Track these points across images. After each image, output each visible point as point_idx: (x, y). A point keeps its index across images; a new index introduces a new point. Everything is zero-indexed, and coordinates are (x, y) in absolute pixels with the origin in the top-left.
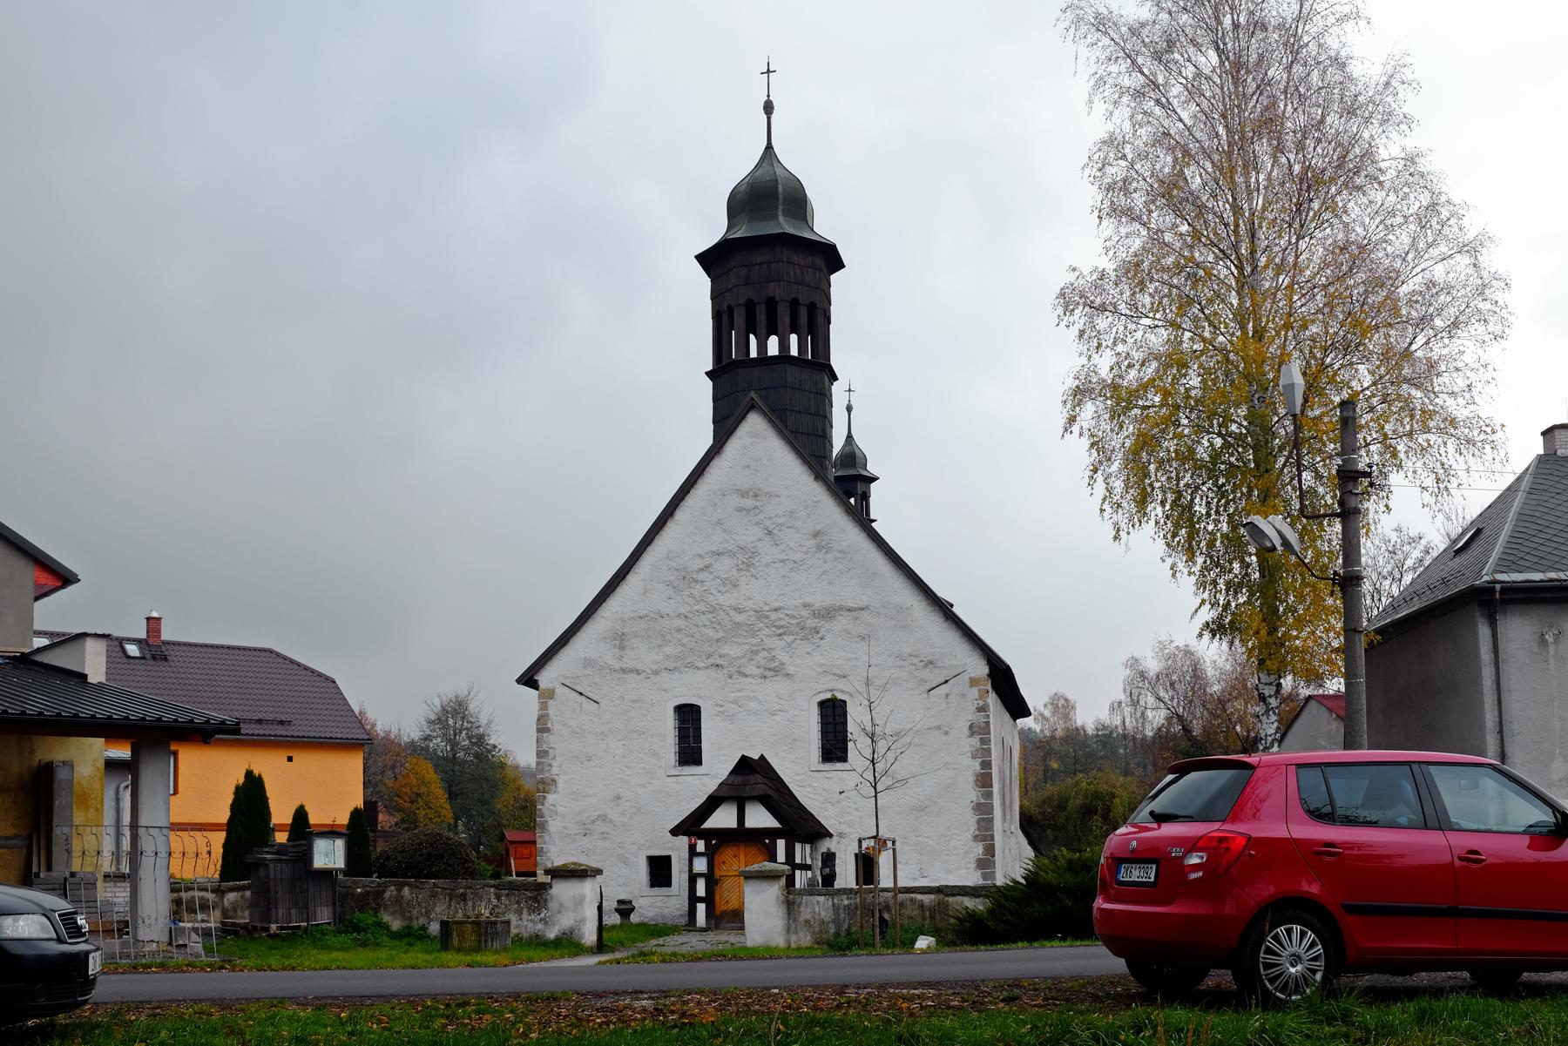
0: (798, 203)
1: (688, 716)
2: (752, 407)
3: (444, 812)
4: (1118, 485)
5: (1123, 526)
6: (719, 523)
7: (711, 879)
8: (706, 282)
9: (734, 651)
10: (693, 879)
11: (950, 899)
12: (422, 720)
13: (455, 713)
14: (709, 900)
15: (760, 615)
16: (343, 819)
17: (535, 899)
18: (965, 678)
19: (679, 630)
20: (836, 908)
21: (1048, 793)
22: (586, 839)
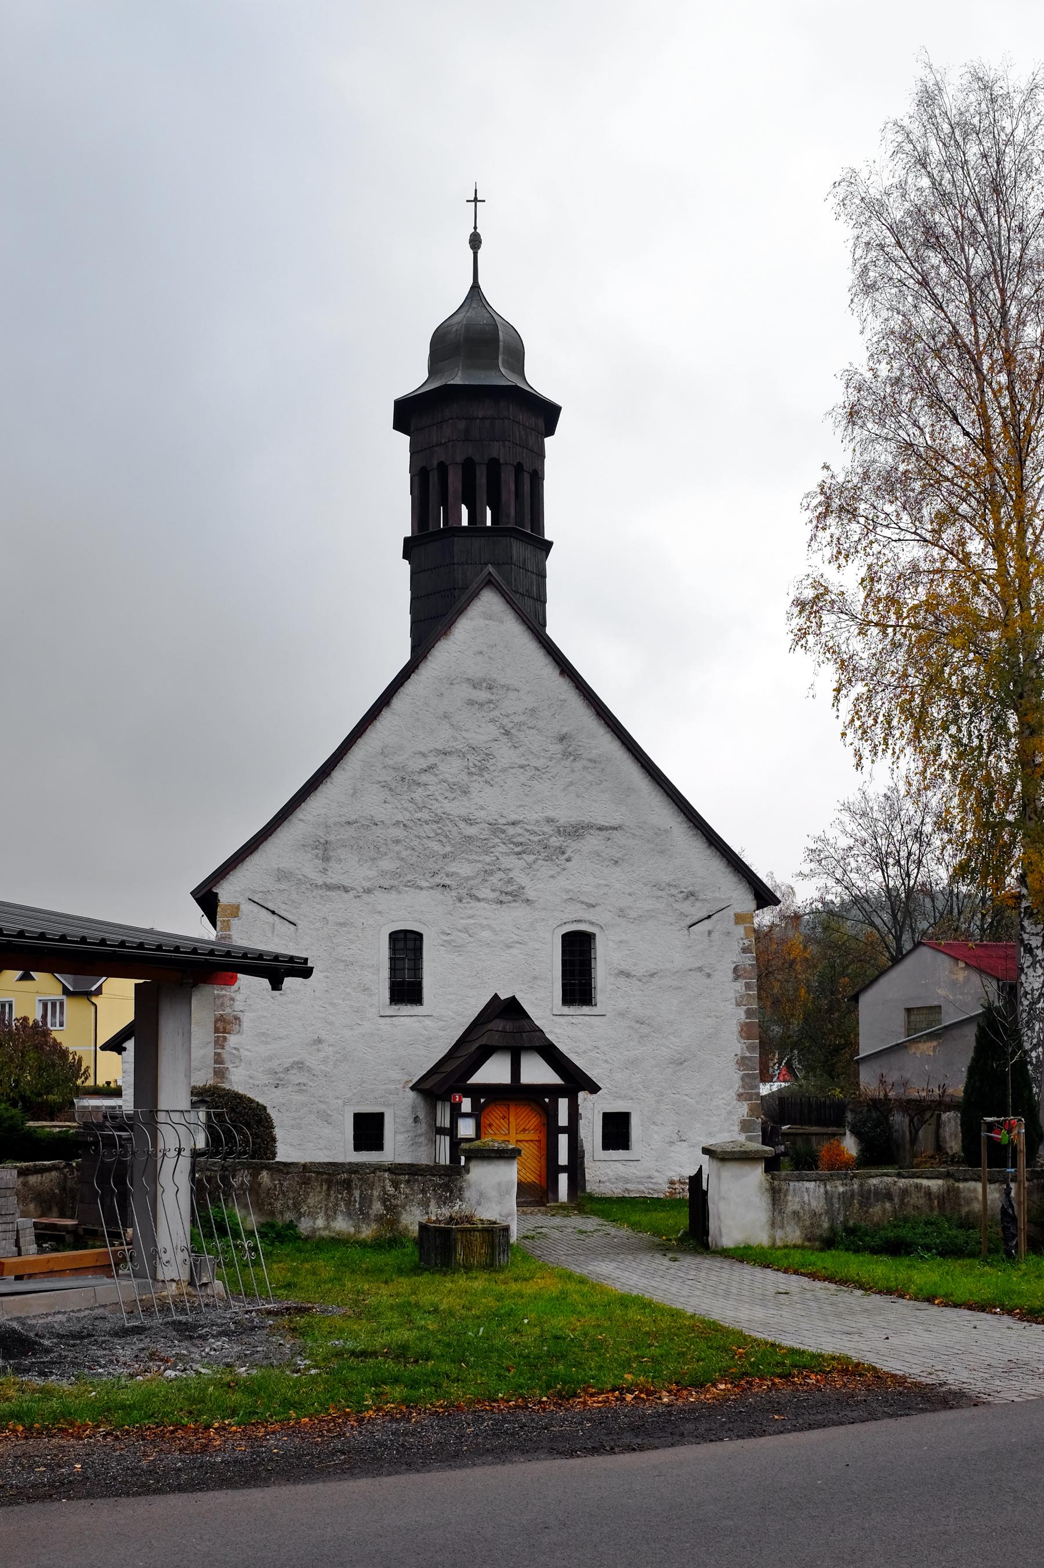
1: (406, 947)
5: (866, 753)
6: (446, 716)
9: (464, 869)
11: (961, 1185)
15: (495, 828)
17: (447, 1187)
18: (730, 913)
19: (398, 842)
20: (828, 1197)
22: (278, 1092)
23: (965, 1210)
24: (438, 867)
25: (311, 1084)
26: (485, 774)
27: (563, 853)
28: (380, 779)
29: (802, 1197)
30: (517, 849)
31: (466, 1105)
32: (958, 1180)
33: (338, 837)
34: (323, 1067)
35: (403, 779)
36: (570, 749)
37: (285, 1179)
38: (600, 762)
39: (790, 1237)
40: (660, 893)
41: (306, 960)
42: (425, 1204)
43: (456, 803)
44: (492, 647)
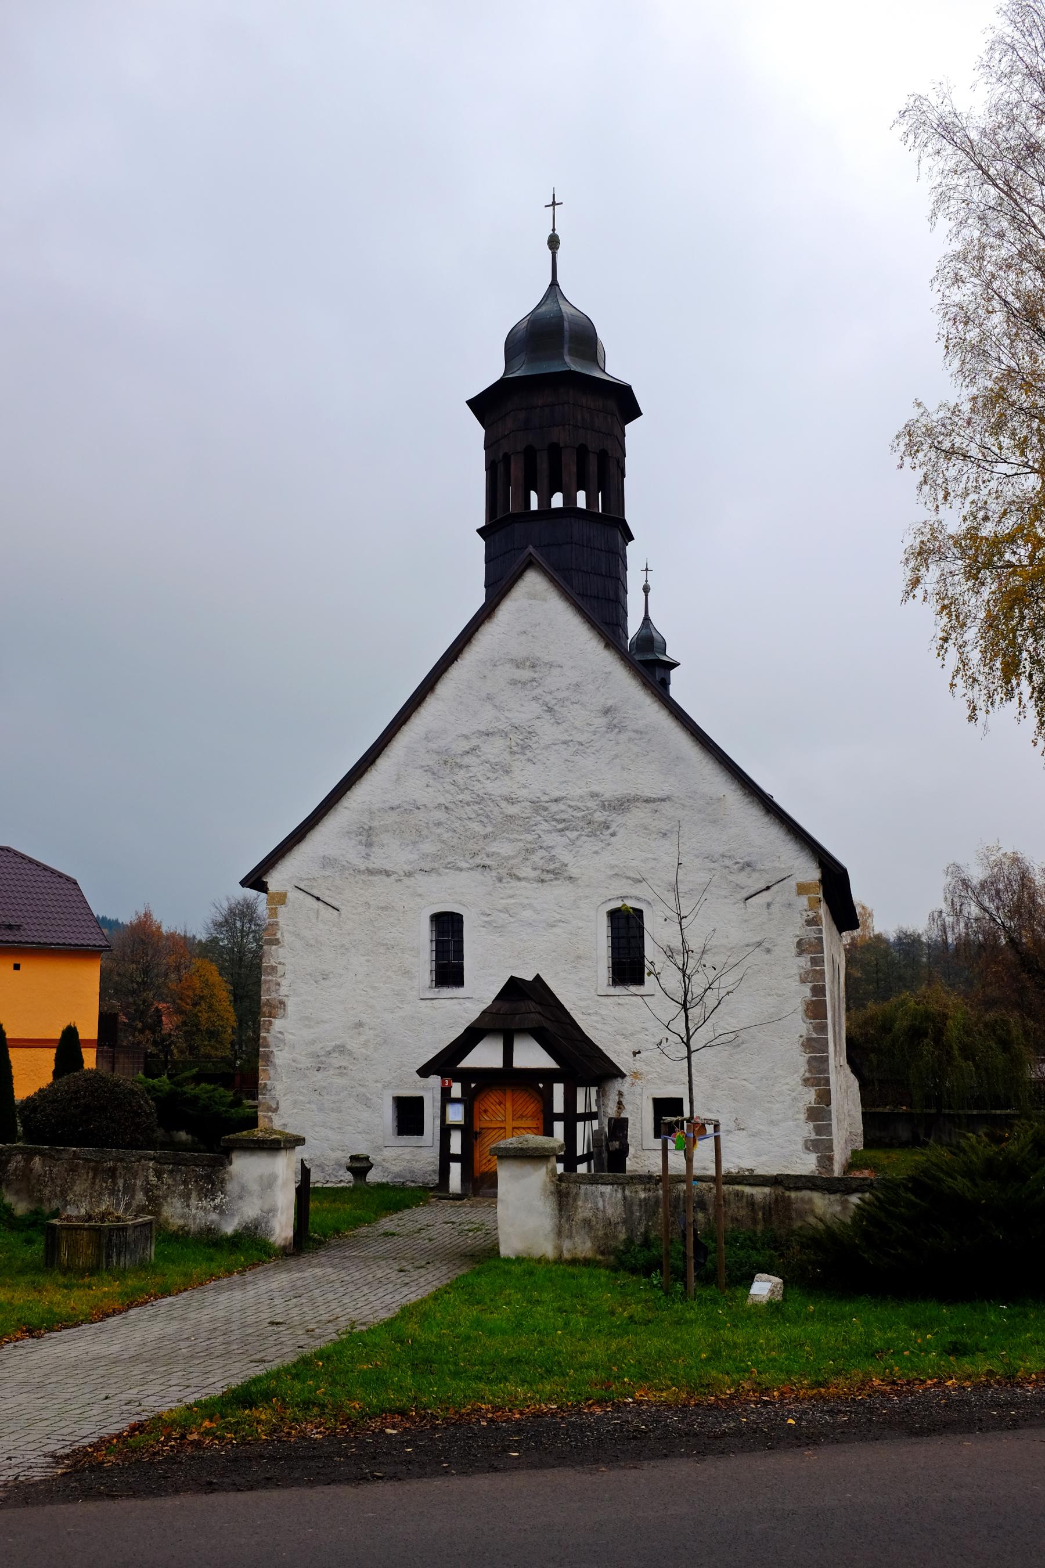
0: (585, 340)
1: (448, 928)
2: (529, 564)
3: (227, 1015)
4: (975, 656)
5: (980, 703)
6: (489, 698)
7: (468, 1130)
8: (478, 432)
9: (503, 848)
10: (446, 1130)
11: (793, 1195)
12: (209, 921)
13: (242, 915)
14: (466, 1158)
15: (537, 806)
16: (58, 1036)
17: (208, 1179)
18: (792, 883)
19: (439, 824)
21: (869, 1012)
22: (320, 1075)
23: (797, 1224)
24: (478, 848)
25: (351, 1067)
26: (527, 752)
27: (608, 828)
28: (423, 764)
29: (596, 1203)
30: (560, 826)
31: (456, 1090)
32: (789, 1189)
33: (382, 823)
34: (364, 1051)
35: (446, 762)
36: (615, 722)
37: (55, 1166)
38: (646, 733)
39: (580, 1249)
40: (713, 865)
41: (276, 942)
42: (186, 1196)
43: (498, 783)
44: (536, 626)
